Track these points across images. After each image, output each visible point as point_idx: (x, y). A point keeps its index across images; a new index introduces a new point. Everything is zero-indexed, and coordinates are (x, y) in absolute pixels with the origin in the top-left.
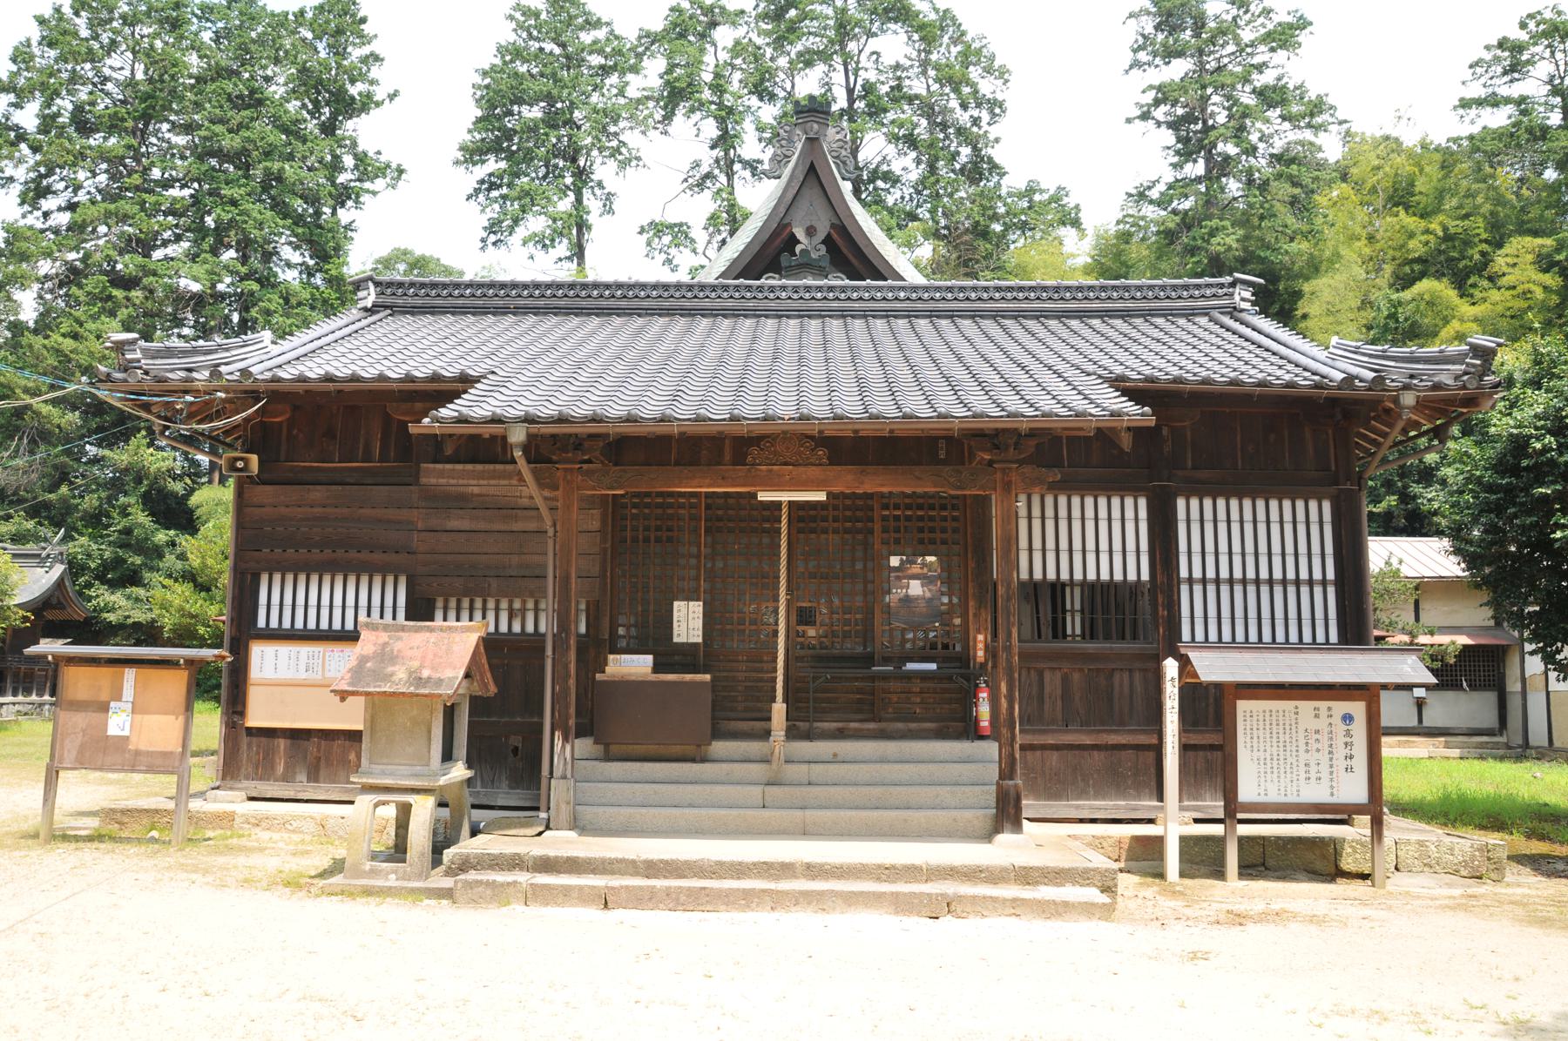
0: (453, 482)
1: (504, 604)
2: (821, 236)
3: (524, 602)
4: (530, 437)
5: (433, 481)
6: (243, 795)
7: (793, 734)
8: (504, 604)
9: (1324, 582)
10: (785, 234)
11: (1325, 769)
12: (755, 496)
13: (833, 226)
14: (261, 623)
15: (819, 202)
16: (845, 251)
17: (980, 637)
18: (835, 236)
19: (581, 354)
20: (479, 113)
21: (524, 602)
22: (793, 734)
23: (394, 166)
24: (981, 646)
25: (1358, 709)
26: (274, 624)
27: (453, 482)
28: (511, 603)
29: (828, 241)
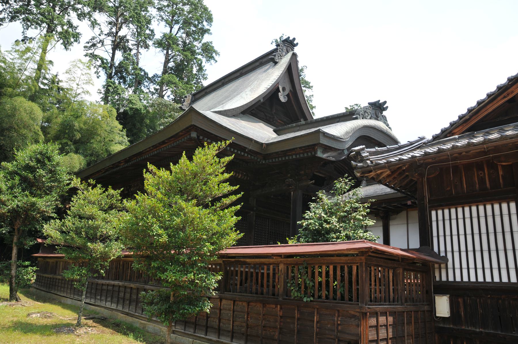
18: (290, 95)
29: (288, 95)
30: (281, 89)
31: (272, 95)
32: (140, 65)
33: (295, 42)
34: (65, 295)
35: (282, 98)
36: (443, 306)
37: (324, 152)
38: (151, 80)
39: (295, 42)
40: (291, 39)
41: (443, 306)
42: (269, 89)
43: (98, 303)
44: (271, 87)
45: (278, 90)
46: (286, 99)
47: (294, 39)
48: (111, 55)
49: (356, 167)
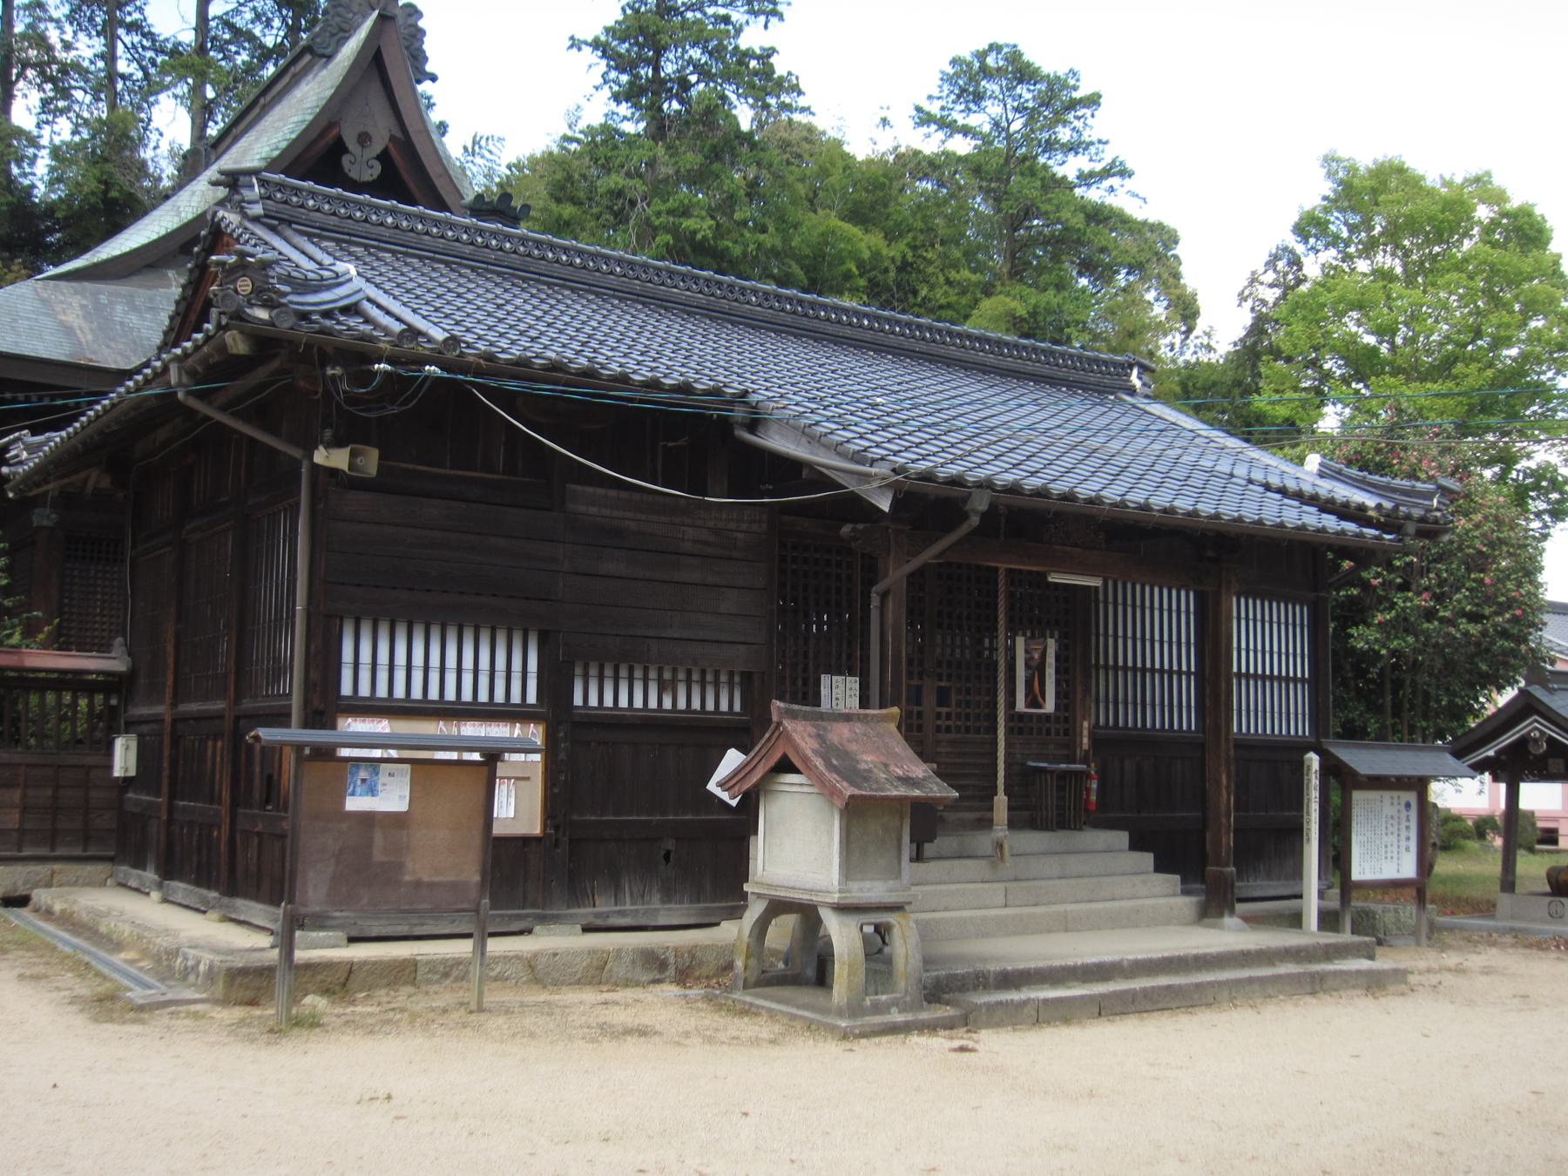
0: (615, 513)
1: (653, 674)
2: (377, 147)
3: (675, 671)
4: (993, 506)
5: (582, 508)
6: (579, 927)
7: (1013, 825)
8: (653, 674)
9: (1188, 673)
10: (335, 132)
11: (1395, 849)
12: (1043, 575)
13: (392, 138)
14: (346, 689)
15: (378, 103)
16: (406, 176)
17: (1086, 724)
18: (394, 153)
19: (1002, 408)
20: (1332, 195)
21: (675, 671)
22: (1013, 825)
23: (1292, 241)
24: (1085, 732)
25: (1411, 797)
26: (364, 691)
27: (615, 513)
28: (660, 671)
29: (384, 157)
30: (351, 143)
46: (377, 169)
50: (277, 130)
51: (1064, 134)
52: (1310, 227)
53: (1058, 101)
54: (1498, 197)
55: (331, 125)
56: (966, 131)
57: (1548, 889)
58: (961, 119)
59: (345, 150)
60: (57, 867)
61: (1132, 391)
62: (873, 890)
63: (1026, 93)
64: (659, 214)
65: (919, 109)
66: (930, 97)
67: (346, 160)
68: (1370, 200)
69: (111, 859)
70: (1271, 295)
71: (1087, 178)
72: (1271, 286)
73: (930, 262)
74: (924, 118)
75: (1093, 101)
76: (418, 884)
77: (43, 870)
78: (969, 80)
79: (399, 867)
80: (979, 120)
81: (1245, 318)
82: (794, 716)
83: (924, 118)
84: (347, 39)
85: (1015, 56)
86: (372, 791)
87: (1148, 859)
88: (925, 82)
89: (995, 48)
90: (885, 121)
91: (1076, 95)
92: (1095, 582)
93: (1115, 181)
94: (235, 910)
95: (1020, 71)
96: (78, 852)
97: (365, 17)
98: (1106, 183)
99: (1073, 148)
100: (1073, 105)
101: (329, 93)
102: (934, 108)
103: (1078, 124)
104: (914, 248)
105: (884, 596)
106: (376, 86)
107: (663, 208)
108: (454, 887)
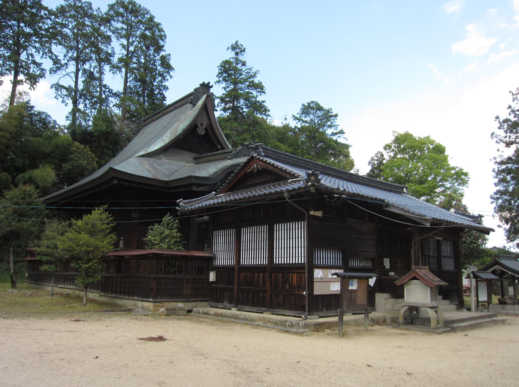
2: (204, 127)
13: (208, 125)
18: (208, 128)
29: (206, 129)
30: (199, 125)
31: (192, 129)
32: (104, 82)
33: (210, 85)
34: (47, 284)
35: (201, 131)
36: (212, 276)
37: (198, 188)
38: (116, 95)
39: (210, 85)
40: (206, 83)
41: (212, 276)
42: (185, 129)
43: (66, 286)
44: (187, 127)
45: (196, 126)
46: (204, 132)
47: (209, 83)
48: (74, 79)
49: (178, 210)
50: (185, 122)
51: (329, 123)
52: (387, 147)
53: (328, 116)
54: (432, 142)
55: (196, 121)
56: (306, 122)
57: (498, 303)
58: (304, 119)
59: (198, 127)
60: (197, 303)
61: (405, 193)
62: (435, 304)
63: (319, 113)
64: (238, 140)
65: (294, 116)
66: (298, 113)
67: (198, 129)
68: (404, 143)
69: (208, 301)
70: (376, 162)
71: (334, 134)
72: (376, 160)
73: (298, 153)
74: (295, 118)
75: (336, 116)
76: (359, 305)
77: (195, 304)
78: (307, 109)
79: (356, 301)
80: (308, 119)
81: (370, 168)
82: (416, 268)
83: (295, 118)
84: (199, 100)
85: (317, 105)
86: (352, 285)
87: (441, 297)
88: (297, 110)
89: (313, 102)
90: (286, 118)
91: (333, 114)
92: (441, 239)
93: (340, 135)
94: (278, 312)
95: (320, 108)
96: (194, 299)
97: (203, 96)
98: (338, 135)
99: (330, 127)
100: (332, 116)
101: (196, 114)
102: (298, 116)
103: (333, 121)
104: (294, 149)
105: (415, 243)
106: (204, 112)
107: (239, 138)
108: (363, 305)
